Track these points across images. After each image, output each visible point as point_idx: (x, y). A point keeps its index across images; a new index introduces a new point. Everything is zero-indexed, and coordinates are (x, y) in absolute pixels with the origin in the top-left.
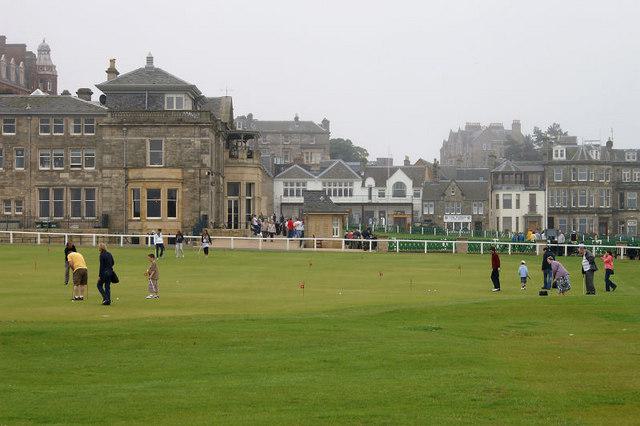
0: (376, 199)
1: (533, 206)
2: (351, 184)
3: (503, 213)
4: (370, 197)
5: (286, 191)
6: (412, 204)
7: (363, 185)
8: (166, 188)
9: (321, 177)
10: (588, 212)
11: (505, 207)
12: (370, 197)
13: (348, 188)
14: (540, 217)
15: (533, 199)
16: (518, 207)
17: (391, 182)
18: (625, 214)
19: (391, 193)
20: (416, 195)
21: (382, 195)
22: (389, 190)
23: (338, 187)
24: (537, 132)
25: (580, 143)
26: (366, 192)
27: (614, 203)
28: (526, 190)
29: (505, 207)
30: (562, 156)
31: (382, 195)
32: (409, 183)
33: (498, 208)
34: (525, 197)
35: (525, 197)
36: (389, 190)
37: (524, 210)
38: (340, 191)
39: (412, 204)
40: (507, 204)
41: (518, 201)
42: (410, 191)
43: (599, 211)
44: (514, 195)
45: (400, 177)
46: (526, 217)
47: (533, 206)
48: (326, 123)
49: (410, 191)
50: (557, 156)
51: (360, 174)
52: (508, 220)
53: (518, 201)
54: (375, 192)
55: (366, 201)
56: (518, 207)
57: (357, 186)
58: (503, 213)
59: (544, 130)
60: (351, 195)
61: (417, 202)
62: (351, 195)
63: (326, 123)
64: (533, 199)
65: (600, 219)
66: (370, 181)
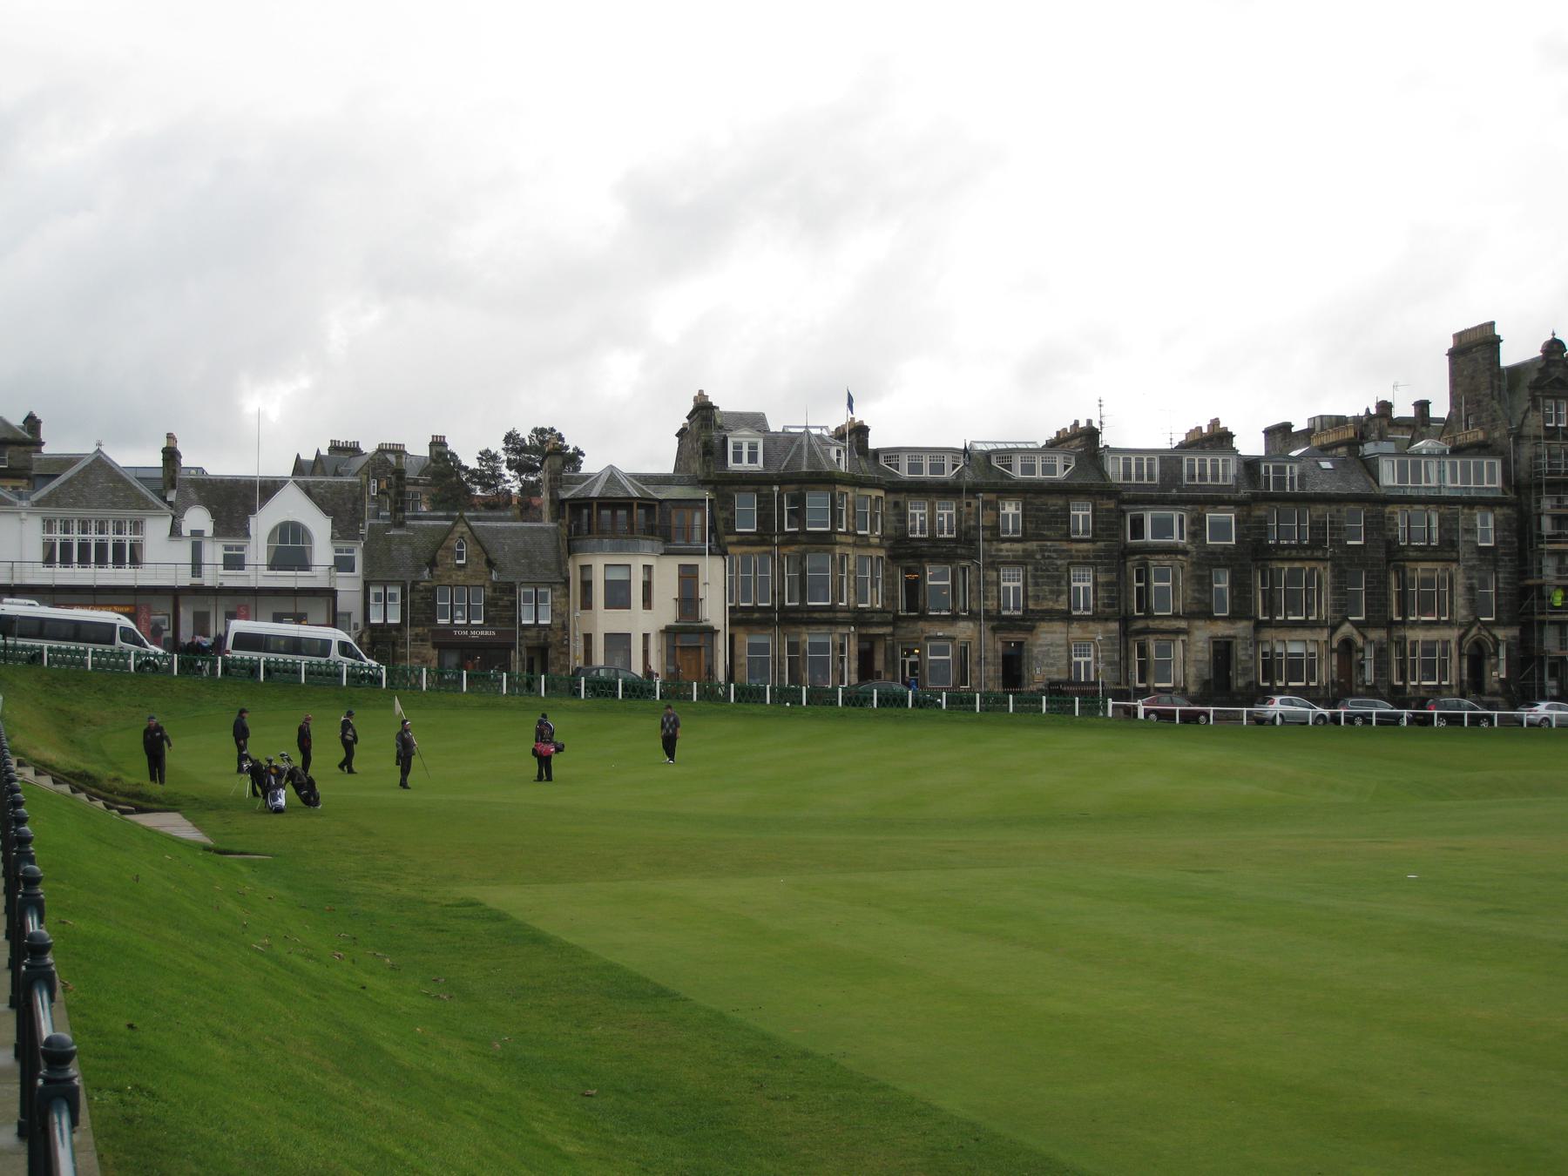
0: (214, 575)
1: (689, 600)
2: (137, 526)
3: (605, 621)
4: (197, 566)
5: (49, 548)
6: (331, 593)
7: (175, 532)
8: (316, 571)
9: (38, 503)
10: (829, 618)
11: (609, 605)
12: (197, 566)
13: (128, 538)
14: (711, 632)
15: (689, 577)
16: (647, 602)
17: (263, 522)
18: (921, 625)
19: (263, 558)
20: (343, 564)
21: (234, 562)
22: (258, 548)
23: (93, 537)
24: (511, 438)
25: (589, 466)
26: (183, 552)
27: (890, 597)
28: (667, 553)
29: (609, 605)
30: (753, 458)
31: (234, 562)
32: (319, 527)
33: (587, 604)
34: (667, 573)
35: (667, 573)
36: (258, 548)
37: (665, 612)
38: (101, 547)
39: (331, 593)
40: (618, 596)
41: (647, 586)
42: (323, 551)
43: (860, 618)
44: (637, 563)
45: (292, 506)
46: (668, 632)
47: (689, 600)
48: (32, 423)
49: (323, 551)
50: (738, 458)
51: (164, 499)
52: (619, 642)
53: (647, 586)
54: (214, 553)
55: (185, 579)
56: (647, 602)
57: (155, 531)
58: (605, 621)
59: (525, 433)
60: (136, 561)
61: (348, 587)
62: (136, 561)
63: (32, 423)
64: (689, 577)
65: (862, 638)
66: (198, 518)
